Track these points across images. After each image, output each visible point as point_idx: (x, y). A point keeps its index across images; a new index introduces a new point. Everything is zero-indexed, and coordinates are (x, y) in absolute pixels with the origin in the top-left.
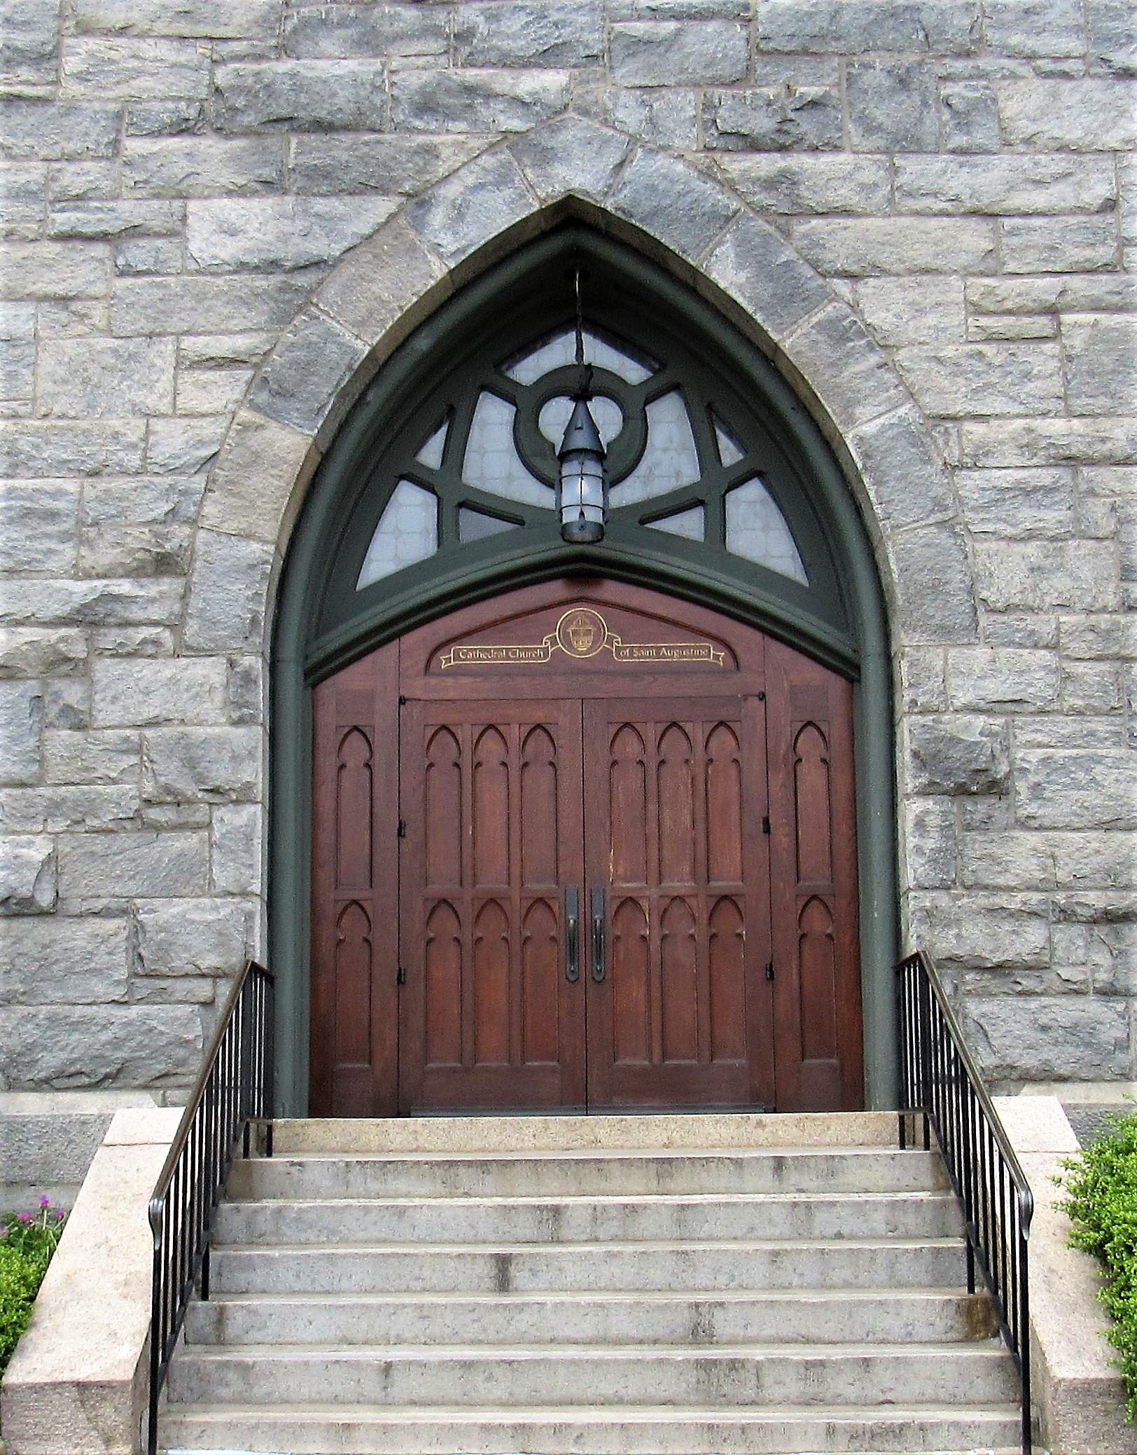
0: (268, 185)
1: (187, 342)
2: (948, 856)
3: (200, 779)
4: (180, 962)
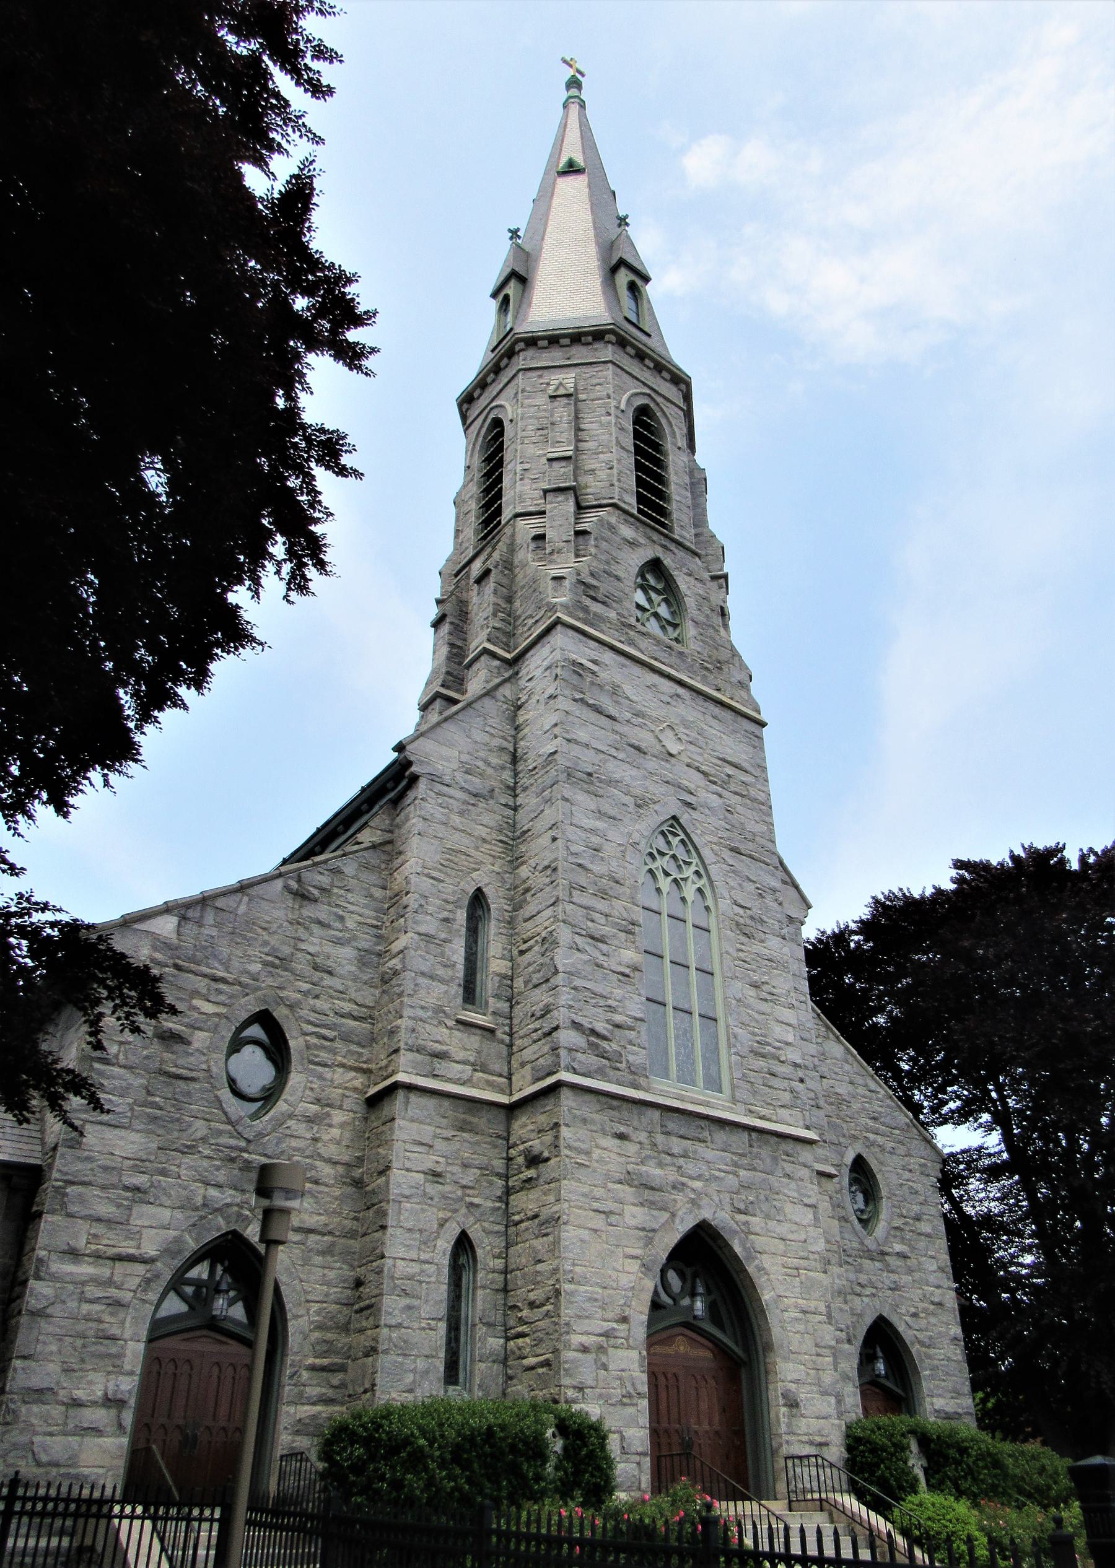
0: (642, 1204)
1: (626, 1249)
2: (789, 1425)
3: (635, 1389)
4: (633, 1450)
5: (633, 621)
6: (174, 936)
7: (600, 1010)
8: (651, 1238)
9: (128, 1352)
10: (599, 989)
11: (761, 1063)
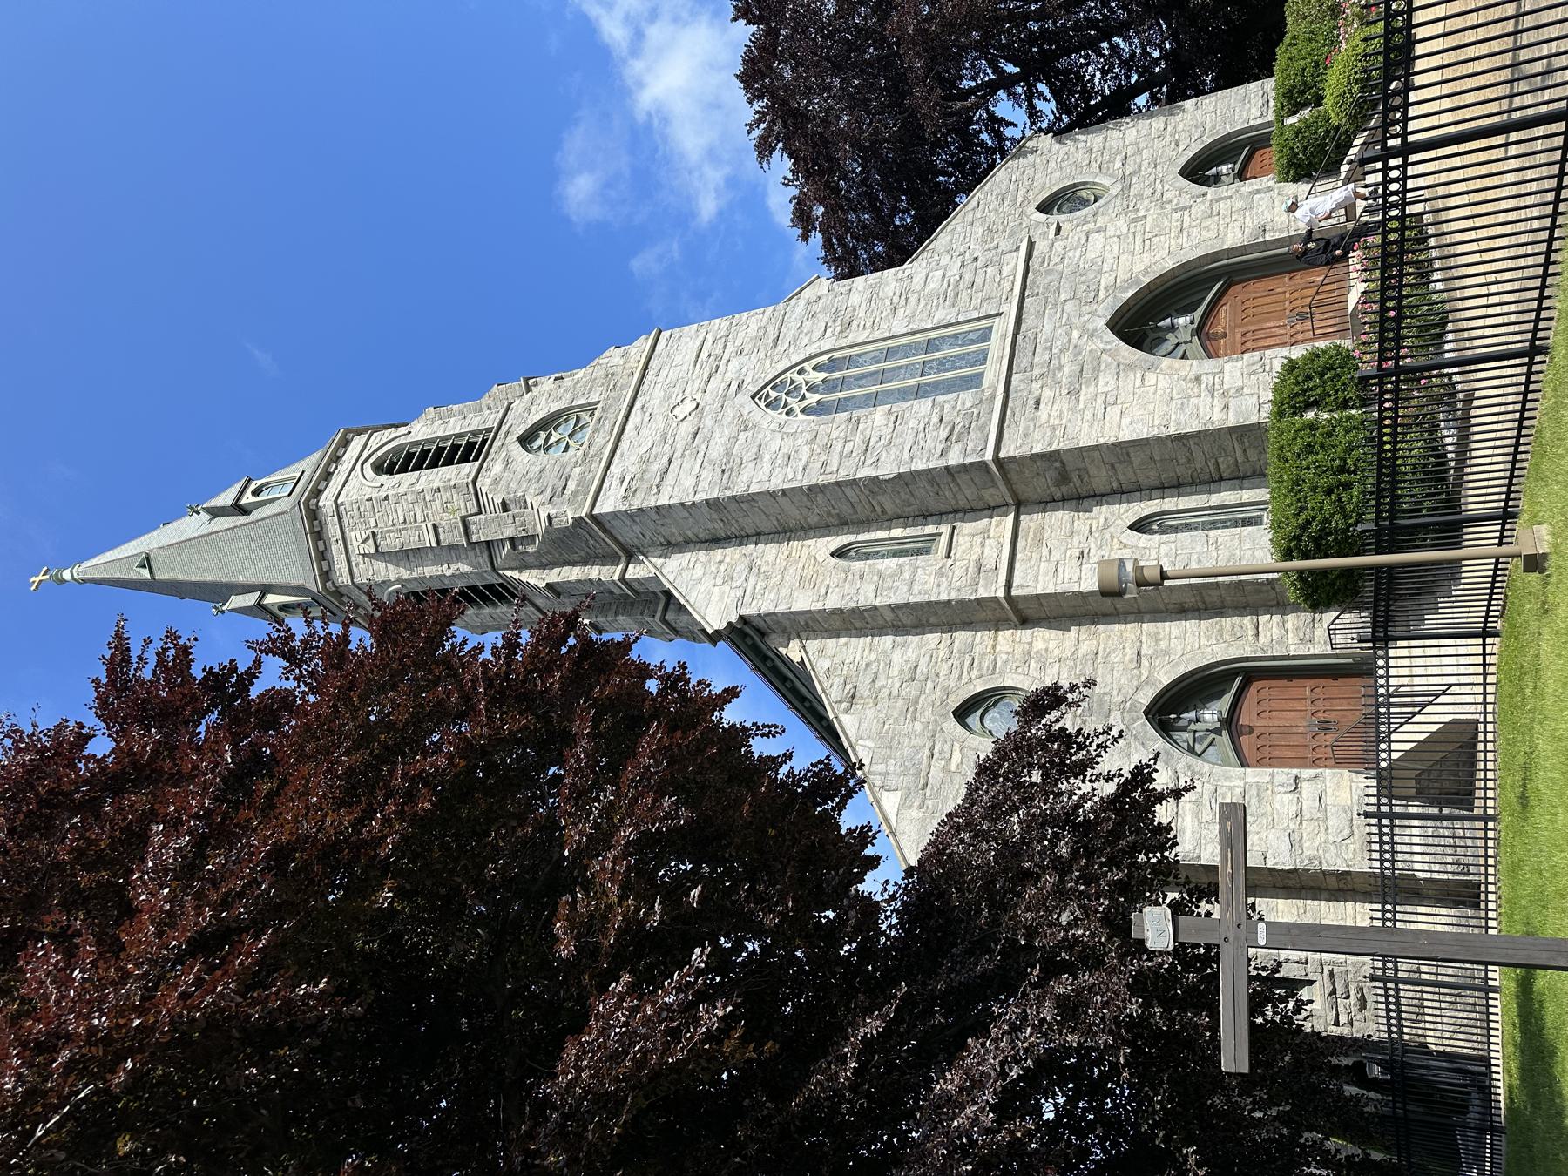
5: (580, 453)
6: (899, 793)
7: (928, 436)
8: (1125, 365)
9: (1256, 780)
10: (911, 439)
11: (964, 296)
